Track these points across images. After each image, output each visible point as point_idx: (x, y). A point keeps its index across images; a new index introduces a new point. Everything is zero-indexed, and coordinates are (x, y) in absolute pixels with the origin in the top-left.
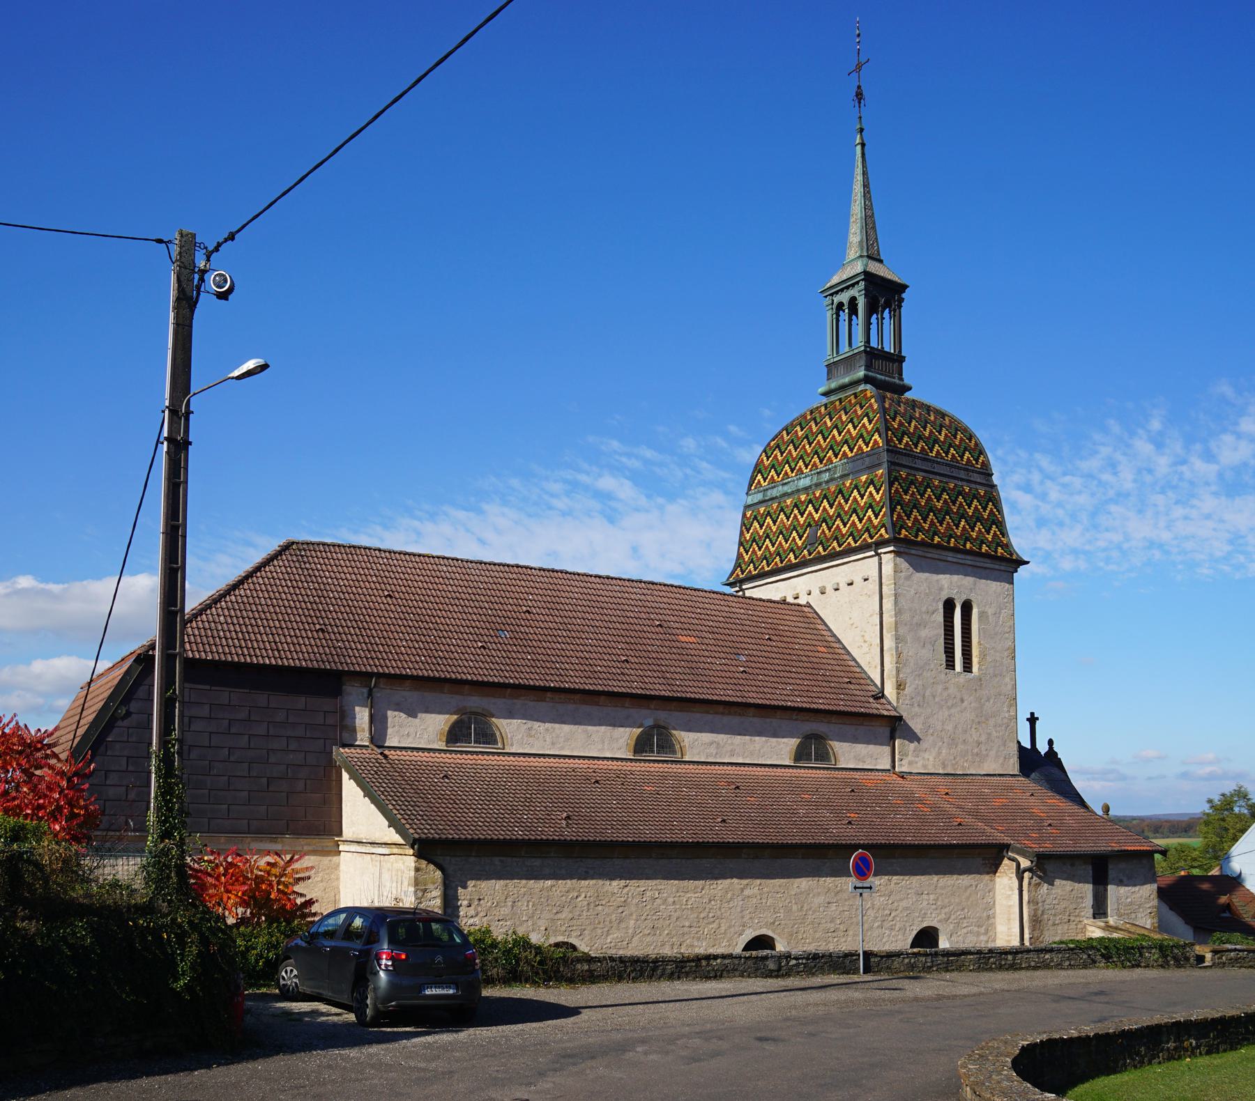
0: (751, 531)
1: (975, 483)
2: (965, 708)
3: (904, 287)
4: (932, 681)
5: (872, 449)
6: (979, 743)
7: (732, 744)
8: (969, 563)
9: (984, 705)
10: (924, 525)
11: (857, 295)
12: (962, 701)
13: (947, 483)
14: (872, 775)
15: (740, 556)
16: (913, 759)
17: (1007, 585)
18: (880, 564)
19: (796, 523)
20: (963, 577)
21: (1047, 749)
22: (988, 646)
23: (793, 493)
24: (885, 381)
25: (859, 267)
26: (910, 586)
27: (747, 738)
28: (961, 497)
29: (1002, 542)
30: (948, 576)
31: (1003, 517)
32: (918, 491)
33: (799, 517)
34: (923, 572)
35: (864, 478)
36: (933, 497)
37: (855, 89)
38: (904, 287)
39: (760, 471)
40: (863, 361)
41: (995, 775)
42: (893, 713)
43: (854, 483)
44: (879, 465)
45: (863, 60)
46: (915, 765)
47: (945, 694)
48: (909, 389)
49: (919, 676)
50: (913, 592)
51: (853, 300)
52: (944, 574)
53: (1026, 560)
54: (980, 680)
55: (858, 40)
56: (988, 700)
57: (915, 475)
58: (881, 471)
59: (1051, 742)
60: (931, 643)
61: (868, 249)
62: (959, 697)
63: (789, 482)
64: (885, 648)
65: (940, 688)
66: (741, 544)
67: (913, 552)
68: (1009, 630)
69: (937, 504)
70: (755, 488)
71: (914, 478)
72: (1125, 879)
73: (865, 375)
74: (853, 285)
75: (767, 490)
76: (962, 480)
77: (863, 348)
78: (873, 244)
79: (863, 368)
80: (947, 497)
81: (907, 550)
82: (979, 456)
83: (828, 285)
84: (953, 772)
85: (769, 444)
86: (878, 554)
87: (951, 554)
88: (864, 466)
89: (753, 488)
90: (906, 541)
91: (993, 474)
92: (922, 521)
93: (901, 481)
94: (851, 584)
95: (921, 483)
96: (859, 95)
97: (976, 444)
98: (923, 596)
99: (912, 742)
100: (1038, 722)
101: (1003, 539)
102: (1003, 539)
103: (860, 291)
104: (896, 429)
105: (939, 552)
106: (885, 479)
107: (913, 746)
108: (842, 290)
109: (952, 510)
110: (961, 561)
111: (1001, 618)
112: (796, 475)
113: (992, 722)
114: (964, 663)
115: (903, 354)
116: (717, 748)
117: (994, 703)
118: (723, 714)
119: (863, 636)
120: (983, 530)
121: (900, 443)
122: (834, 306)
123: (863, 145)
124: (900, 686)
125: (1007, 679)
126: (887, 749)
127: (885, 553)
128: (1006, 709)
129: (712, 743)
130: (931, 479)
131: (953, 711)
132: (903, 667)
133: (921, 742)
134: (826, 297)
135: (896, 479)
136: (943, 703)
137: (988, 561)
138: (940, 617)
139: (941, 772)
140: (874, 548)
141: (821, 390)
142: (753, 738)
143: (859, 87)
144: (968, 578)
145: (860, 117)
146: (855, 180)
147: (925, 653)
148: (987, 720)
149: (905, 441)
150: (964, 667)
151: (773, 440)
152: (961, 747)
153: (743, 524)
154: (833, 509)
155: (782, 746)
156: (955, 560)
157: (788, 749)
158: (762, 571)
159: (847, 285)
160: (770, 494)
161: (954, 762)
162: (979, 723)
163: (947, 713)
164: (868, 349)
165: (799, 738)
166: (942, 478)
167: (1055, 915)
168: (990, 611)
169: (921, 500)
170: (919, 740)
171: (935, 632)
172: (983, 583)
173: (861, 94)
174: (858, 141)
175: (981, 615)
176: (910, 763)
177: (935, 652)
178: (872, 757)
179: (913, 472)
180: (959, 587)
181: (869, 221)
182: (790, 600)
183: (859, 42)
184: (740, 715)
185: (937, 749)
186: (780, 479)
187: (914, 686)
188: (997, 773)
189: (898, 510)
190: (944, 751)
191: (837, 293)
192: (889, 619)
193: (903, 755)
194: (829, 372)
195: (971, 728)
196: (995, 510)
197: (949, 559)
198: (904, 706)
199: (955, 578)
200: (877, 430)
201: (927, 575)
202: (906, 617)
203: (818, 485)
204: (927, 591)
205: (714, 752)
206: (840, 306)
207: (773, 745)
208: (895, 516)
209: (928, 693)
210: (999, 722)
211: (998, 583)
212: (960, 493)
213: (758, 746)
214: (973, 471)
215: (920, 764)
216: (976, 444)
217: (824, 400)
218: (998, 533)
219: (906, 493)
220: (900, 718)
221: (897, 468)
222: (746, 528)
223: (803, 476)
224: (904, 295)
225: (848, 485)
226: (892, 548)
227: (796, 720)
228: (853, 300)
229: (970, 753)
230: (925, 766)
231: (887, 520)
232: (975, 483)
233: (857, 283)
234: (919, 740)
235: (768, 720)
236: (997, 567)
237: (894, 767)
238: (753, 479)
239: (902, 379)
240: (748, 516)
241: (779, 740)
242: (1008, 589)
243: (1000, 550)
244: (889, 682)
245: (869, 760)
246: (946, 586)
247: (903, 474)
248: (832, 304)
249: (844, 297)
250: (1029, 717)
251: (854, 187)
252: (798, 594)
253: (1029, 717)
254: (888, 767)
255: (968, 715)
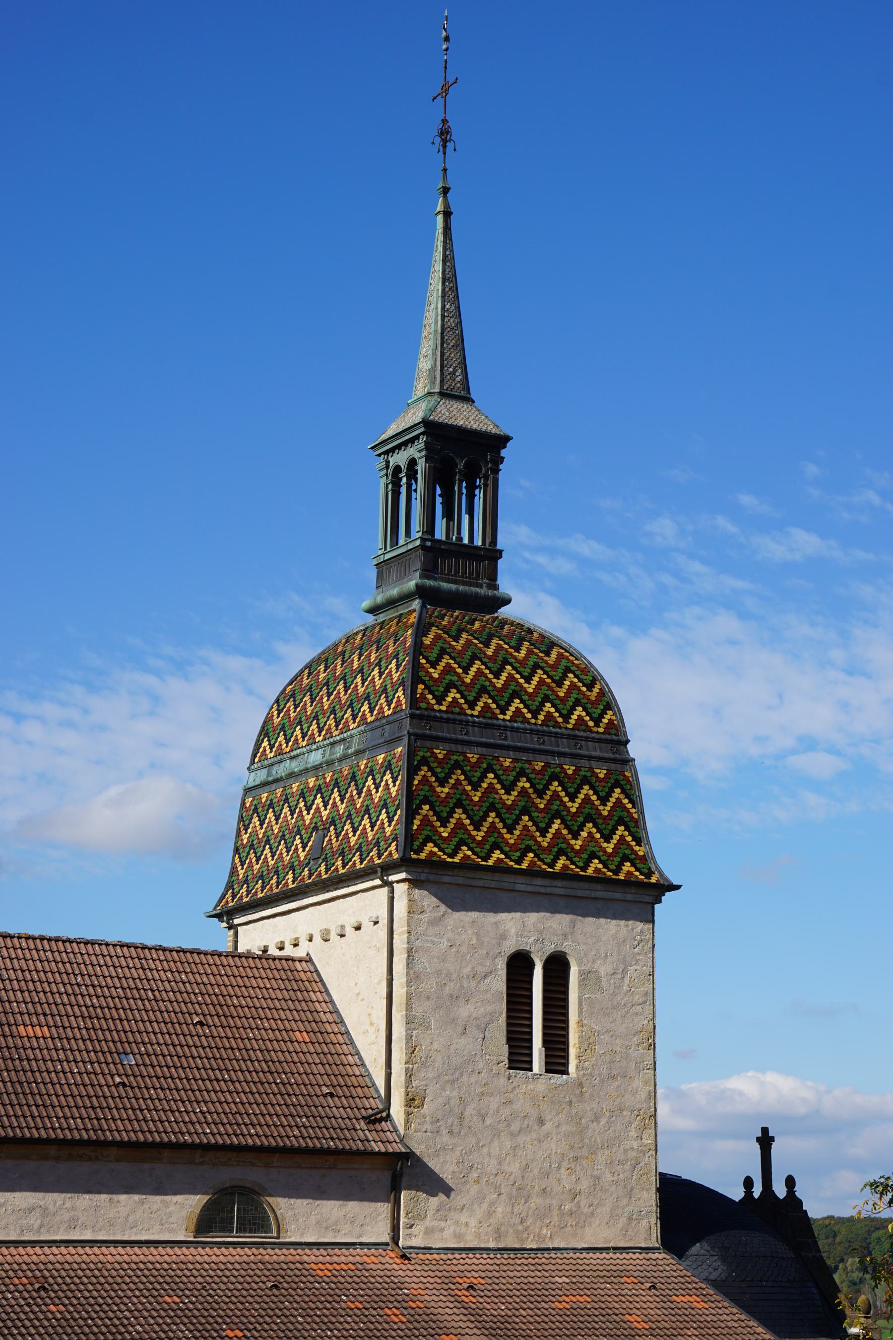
0: (249, 831)
1: (589, 758)
2: (548, 1135)
3: (503, 440)
4: (480, 1090)
5: (394, 713)
6: (575, 1195)
7: (73, 1208)
9: (587, 1127)
10: (474, 833)
11: (417, 455)
12: (541, 1122)
13: (528, 762)
14: (343, 1256)
15: (234, 871)
16: (435, 1223)
17: (640, 926)
18: (391, 899)
19: (300, 823)
20: (548, 914)
21: (743, 1195)
22: (597, 1028)
23: (301, 773)
24: (457, 591)
25: (415, 415)
26: (440, 935)
27: (104, 1197)
28: (556, 783)
29: (636, 853)
30: (519, 914)
31: (641, 812)
32: (467, 778)
33: (305, 813)
34: (467, 909)
35: (380, 758)
36: (498, 786)
37: (438, 125)
38: (503, 440)
39: (267, 735)
40: (417, 564)
41: (608, 1249)
42: (400, 1148)
43: (369, 765)
44: (397, 740)
45: (451, 80)
46: (437, 1235)
48: (507, 601)
49: (453, 1082)
50: (445, 944)
51: (412, 462)
52: (509, 911)
53: (675, 883)
54: (581, 1085)
55: (444, 47)
56: (596, 1119)
57: (464, 754)
58: (400, 749)
59: (790, 1182)
60: (478, 1027)
61: (442, 381)
62: (534, 1115)
63: (298, 756)
64: (394, 1037)
65: (494, 1103)
66: (237, 851)
67: (446, 879)
68: (641, 1000)
69: (505, 797)
70: (260, 761)
71: (461, 758)
73: (417, 586)
74: (412, 440)
75: (272, 765)
76: (561, 754)
77: (418, 543)
78: (455, 371)
79: (418, 574)
80: (527, 785)
81: (432, 877)
82: (604, 712)
83: (380, 440)
84: (517, 1246)
85: (285, 689)
86: (390, 884)
88: (382, 740)
89: (256, 760)
90: (431, 863)
91: (628, 741)
92: (470, 828)
93: (434, 765)
94: (358, 928)
95: (475, 766)
96: (445, 134)
97: (602, 693)
98: (464, 949)
99: (434, 1194)
100: (774, 1146)
101: (637, 848)
102: (637, 848)
103: (420, 451)
104: (435, 680)
105: (497, 876)
106: (403, 763)
107: (434, 1202)
108: (399, 447)
110: (543, 890)
111: (627, 981)
112: (308, 745)
113: (602, 1157)
114: (546, 1056)
115: (499, 547)
116: (43, 1216)
117: (609, 1124)
118: (57, 1159)
119: (370, 1015)
120: (598, 836)
122: (390, 471)
123: (447, 214)
124: (410, 1101)
125: (637, 1083)
126: (383, 1209)
127: (398, 882)
128: (633, 1134)
129: (32, 1209)
130: (497, 758)
131: (521, 1139)
132: (419, 1070)
133: (453, 1195)
134: (379, 455)
135: (424, 761)
136: (501, 1126)
137: (599, 887)
138: (499, 983)
139: (492, 1245)
140: (379, 874)
141: (366, 604)
142: (116, 1197)
143: (444, 121)
144: (558, 916)
145: (445, 170)
146: (432, 270)
147: (467, 1045)
148: (594, 1153)
149: (449, 699)
150: (547, 1063)
151: (291, 683)
152: (536, 1201)
153: (241, 819)
154: (344, 805)
155: (172, 1208)
156: (530, 889)
157: (184, 1213)
158: (284, 889)
159: (402, 441)
160: (280, 770)
161: (520, 1228)
162: (576, 1159)
163: (508, 1144)
164: (429, 544)
166: (518, 755)
168: (604, 970)
169: (472, 793)
170: (447, 1190)
171: (490, 1008)
172: (589, 924)
173: (448, 132)
174: (440, 207)
175: (584, 977)
176: (428, 1232)
177: (487, 1042)
178: (352, 1222)
179: (460, 748)
180: (539, 932)
181: (449, 335)
182: (273, 951)
183: (447, 49)
184: (90, 1159)
185: (485, 1206)
186: (288, 749)
187: (441, 1100)
188: (612, 1245)
189: (423, 812)
190: (500, 1210)
191: (392, 450)
192: (399, 991)
193: (413, 1218)
194: (380, 576)
195: (559, 1167)
196: (626, 801)
197: (519, 887)
198: (419, 1134)
199: (533, 918)
200: (403, 683)
201: (474, 915)
202: (429, 985)
203: (330, 763)
204: (474, 941)
205: (37, 1224)
207: (155, 1207)
208: (417, 822)
209: (470, 1111)
210: (620, 1156)
211: (623, 922)
212: (554, 777)
213: (123, 1211)
214: (587, 739)
215: (448, 1233)
216: (602, 693)
217: (370, 619)
218: (629, 838)
219: (442, 783)
220: (409, 1156)
221: (428, 744)
222: (244, 825)
223: (314, 747)
224: (503, 453)
225: (362, 767)
226: (403, 875)
227: (202, 1163)
228: (412, 462)
229: (555, 1212)
230: (458, 1236)
231: (401, 830)
232: (589, 758)
233: (417, 437)
234: (447, 1190)
235: (147, 1166)
236: (618, 896)
237: (395, 1239)
238: (258, 745)
239: (495, 587)
240: (248, 805)
241: (168, 1198)
242: (642, 932)
243: (627, 867)
244: (397, 1093)
245: (347, 1228)
246: (513, 931)
247: (440, 753)
248: (387, 467)
249: (400, 459)
250: (760, 1135)
251: (431, 281)
252: (297, 939)
253: (760, 1135)
254: (386, 1238)
255: (554, 1146)
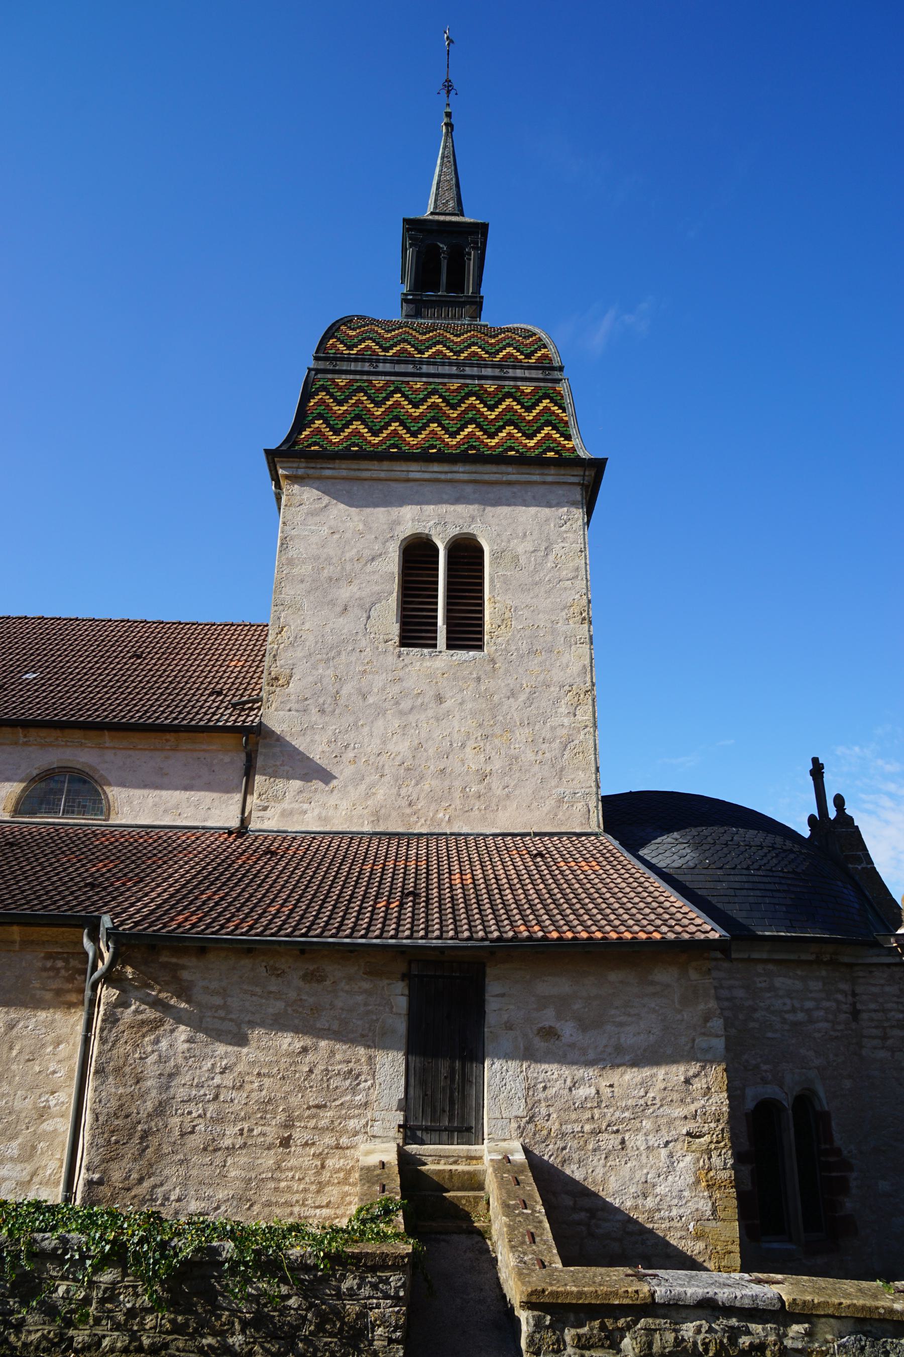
4: (361, 669)
8: (465, 477)
9: (500, 704)
47: (396, 689)
67: (328, 473)
72: (568, 1030)
87: (414, 466)
156: (427, 476)
165: (21, 781)
167: (219, 1120)
176: (285, 814)
195: (463, 746)
197: (412, 475)
227: (25, 744)
234: (326, 776)
245: (190, 811)
255: (456, 724)
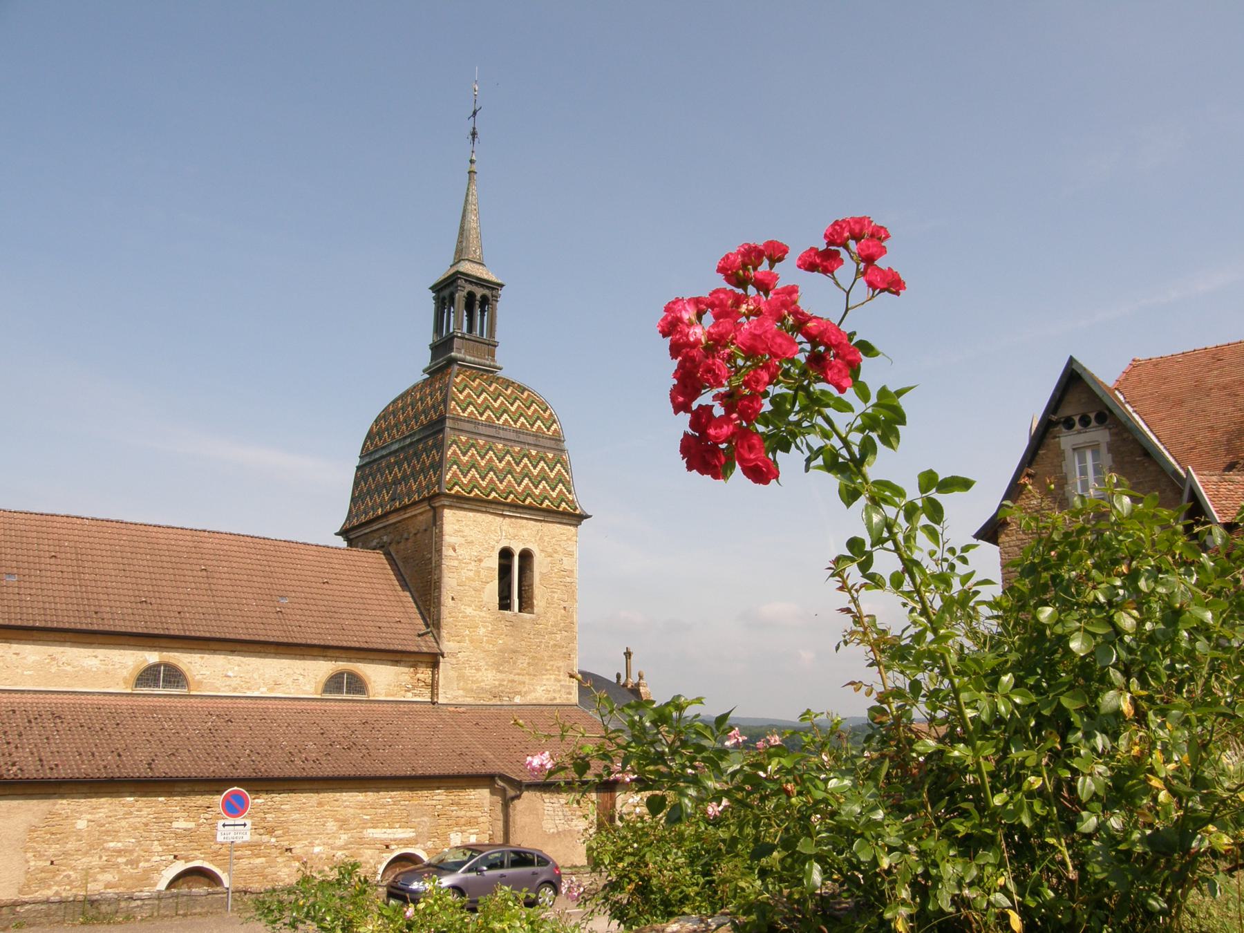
13: (511, 447)
67: (466, 506)
69: (498, 464)
95: (482, 447)
96: (474, 134)
109: (515, 470)
121: (548, 431)
143: (474, 128)
196: (563, 471)
206: (444, 298)
214: (530, 435)
216: (551, 415)
243: (564, 505)
247: (463, 439)
